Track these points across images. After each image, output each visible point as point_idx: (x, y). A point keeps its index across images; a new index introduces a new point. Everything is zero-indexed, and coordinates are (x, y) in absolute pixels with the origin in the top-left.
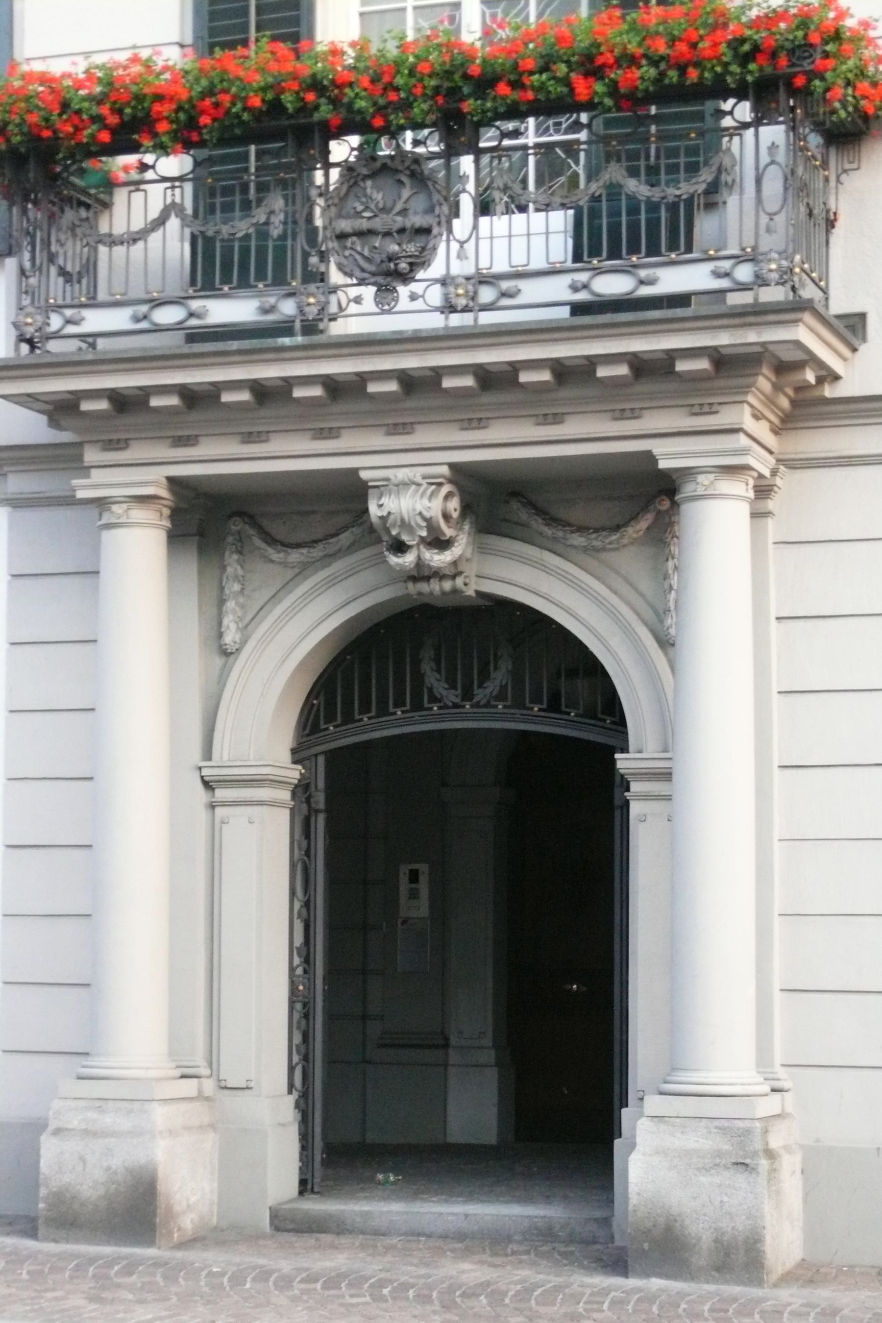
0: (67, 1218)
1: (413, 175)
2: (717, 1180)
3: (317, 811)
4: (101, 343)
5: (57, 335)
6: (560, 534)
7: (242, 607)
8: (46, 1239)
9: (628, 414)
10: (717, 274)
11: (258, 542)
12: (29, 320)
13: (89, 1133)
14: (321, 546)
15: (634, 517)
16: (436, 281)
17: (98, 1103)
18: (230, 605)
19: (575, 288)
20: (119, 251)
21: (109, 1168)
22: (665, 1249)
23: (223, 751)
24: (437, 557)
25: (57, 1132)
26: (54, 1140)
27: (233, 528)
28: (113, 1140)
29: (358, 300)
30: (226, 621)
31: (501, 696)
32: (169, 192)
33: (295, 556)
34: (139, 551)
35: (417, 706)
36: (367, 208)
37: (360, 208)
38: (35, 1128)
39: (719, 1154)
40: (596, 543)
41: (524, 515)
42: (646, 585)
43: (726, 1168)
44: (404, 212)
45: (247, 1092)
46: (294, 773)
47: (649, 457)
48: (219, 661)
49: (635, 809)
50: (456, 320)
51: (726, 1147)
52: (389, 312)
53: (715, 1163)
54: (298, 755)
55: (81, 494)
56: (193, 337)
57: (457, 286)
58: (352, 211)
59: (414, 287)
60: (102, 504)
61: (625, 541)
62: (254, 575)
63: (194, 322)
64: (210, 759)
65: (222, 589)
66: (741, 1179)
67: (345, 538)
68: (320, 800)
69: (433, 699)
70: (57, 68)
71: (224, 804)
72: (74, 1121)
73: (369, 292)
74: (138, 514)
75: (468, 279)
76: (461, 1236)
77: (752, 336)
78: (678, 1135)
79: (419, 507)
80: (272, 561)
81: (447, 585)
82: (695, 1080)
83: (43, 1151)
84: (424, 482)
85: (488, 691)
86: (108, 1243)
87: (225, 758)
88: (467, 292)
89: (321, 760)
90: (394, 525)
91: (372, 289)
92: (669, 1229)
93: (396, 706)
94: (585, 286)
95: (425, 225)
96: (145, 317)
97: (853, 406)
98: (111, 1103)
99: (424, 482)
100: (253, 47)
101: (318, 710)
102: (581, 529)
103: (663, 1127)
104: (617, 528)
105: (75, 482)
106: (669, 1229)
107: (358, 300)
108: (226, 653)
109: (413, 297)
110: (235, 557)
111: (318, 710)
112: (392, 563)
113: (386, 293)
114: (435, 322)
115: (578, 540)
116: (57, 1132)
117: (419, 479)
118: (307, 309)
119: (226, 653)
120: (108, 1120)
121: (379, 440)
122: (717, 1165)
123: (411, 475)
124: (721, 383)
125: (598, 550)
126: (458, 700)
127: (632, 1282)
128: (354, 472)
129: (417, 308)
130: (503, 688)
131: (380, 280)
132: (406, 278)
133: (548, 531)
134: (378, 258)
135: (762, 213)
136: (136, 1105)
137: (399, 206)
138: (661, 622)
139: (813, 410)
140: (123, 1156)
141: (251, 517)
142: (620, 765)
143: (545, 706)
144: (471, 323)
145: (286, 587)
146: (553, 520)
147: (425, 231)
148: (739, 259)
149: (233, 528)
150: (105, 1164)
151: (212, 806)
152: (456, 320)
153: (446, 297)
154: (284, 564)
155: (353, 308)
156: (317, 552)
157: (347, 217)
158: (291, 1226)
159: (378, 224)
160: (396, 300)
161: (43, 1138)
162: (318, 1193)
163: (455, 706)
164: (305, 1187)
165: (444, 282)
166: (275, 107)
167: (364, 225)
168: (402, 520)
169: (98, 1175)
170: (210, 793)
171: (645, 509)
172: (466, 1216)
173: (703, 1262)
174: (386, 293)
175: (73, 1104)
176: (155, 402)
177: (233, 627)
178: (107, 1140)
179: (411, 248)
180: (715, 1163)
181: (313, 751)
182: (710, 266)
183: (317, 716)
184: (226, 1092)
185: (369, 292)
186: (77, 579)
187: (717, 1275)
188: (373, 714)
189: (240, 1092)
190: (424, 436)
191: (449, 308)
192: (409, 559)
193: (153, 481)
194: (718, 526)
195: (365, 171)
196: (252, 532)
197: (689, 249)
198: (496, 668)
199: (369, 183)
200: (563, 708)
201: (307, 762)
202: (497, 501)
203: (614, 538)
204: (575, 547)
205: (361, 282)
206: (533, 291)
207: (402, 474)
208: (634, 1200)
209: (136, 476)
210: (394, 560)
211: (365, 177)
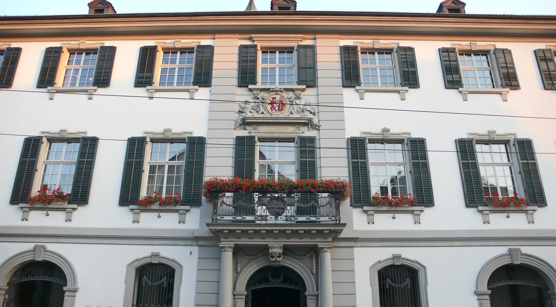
5: (219, 220)
15: (307, 254)
20: (322, 208)
23: (237, 289)
31: (282, 281)
33: (250, 257)
34: (228, 256)
35: (267, 283)
46: (246, 293)
50: (288, 222)
54: (247, 289)
60: (223, 247)
67: (259, 255)
68: (250, 298)
70: (224, 178)
73: (273, 217)
74: (230, 249)
100: (256, 43)
108: (237, 273)
113: (276, 218)
114: (285, 222)
115: (299, 257)
119: (237, 273)
121: (272, 240)
129: (281, 220)
132: (280, 215)
146: (294, 254)
151: (234, 299)
152: (288, 222)
156: (254, 257)
159: (275, 207)
165: (286, 216)
166: (262, 188)
174: (276, 218)
185: (273, 217)
191: (287, 220)
193: (232, 244)
194: (327, 256)
207: (275, 245)
209: (228, 244)
210: (271, 259)
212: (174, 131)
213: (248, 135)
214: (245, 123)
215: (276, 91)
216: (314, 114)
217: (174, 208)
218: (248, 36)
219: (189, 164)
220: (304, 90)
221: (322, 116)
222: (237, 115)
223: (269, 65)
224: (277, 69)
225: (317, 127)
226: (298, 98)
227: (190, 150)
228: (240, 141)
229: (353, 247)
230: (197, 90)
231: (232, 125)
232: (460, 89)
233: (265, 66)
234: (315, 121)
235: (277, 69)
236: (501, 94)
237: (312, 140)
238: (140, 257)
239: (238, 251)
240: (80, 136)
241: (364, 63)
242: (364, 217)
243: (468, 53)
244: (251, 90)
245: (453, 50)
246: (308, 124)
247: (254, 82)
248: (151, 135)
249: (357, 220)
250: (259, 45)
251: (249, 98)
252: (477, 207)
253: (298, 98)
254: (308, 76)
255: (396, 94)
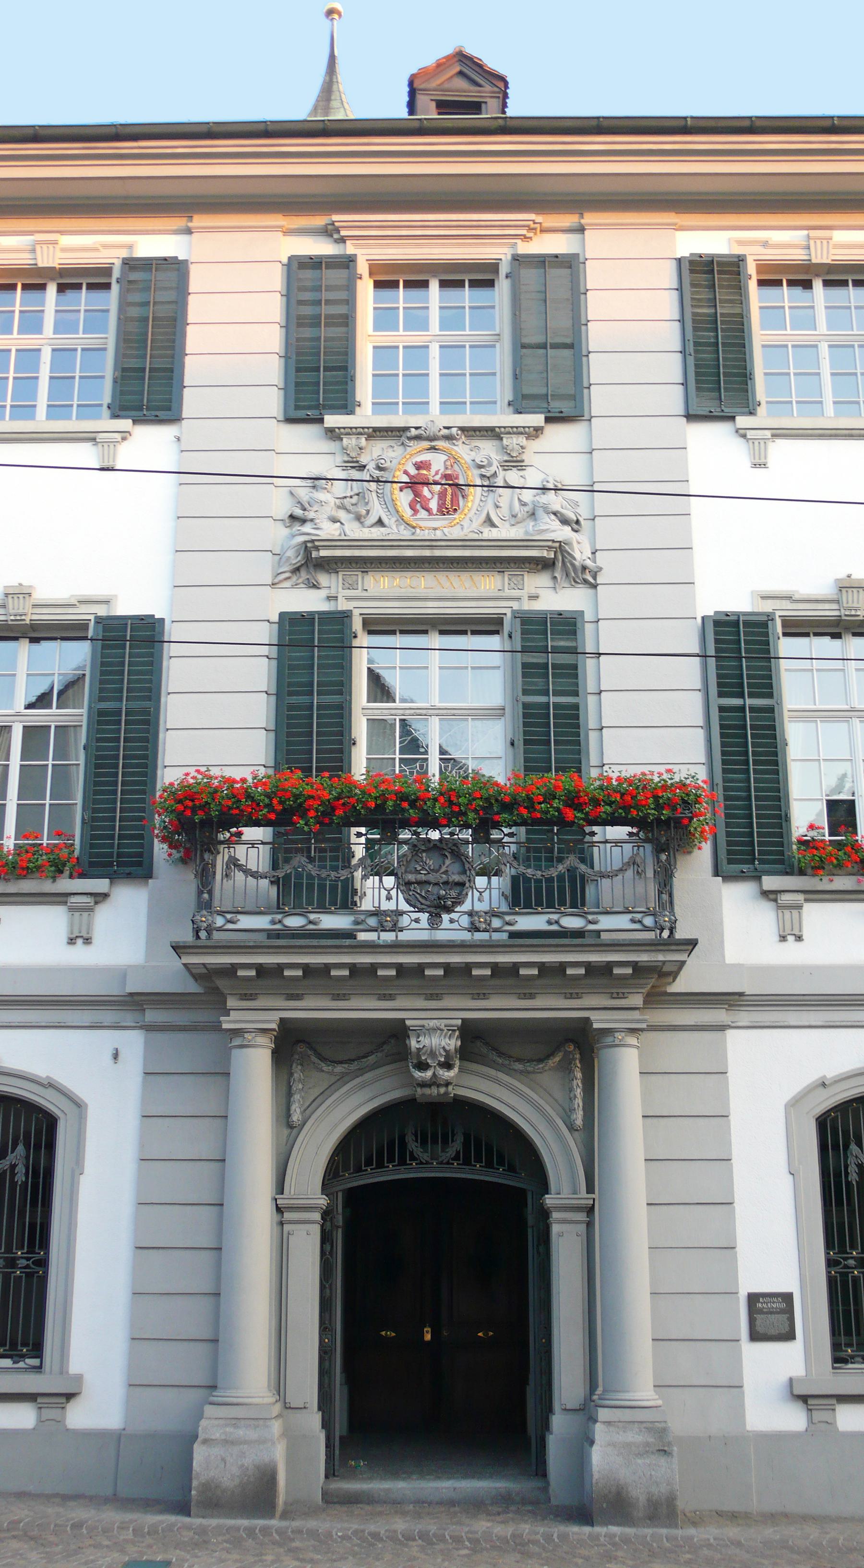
0: (215, 1502)
1: (452, 852)
2: (648, 1461)
3: (338, 1227)
4: (604, 936)
6: (507, 1062)
7: (303, 1098)
8: (198, 1516)
9: (481, 996)
10: (633, 921)
11: (314, 1059)
12: (204, 919)
13: (227, 1442)
14: (356, 1063)
16: (465, 913)
17: (234, 1422)
18: (297, 1097)
19: (549, 922)
20: (605, 883)
21: (243, 1466)
22: (616, 1506)
24: (446, 1074)
25: (205, 1441)
26: (204, 1448)
27: (299, 1049)
28: (246, 1446)
29: (417, 921)
30: (293, 1107)
31: (456, 1158)
32: (226, 850)
33: (339, 1069)
34: (256, 1064)
35: (402, 1162)
36: (423, 869)
37: (419, 868)
38: (188, 1440)
39: (647, 1444)
40: (529, 1069)
41: (484, 1050)
42: (558, 1095)
43: (652, 1453)
44: (446, 872)
45: (304, 1410)
47: (587, 1020)
48: (286, 1131)
49: (555, 1229)
50: (479, 936)
51: (651, 1440)
52: (437, 929)
53: (645, 1451)
55: (225, 1026)
56: (513, 935)
57: (479, 917)
58: (413, 870)
59: (454, 916)
60: (237, 1032)
61: (547, 1068)
62: (308, 1081)
63: (311, 927)
64: (282, 1193)
65: (290, 1087)
66: (663, 1461)
67: (372, 1059)
68: (340, 1220)
69: (413, 1158)
70: (237, 774)
71: (291, 1222)
72: (217, 1435)
75: (486, 913)
76: (452, 1503)
77: (661, 957)
78: (621, 1433)
79: (443, 1044)
80: (323, 1071)
81: (442, 1090)
82: (627, 1398)
83: (195, 1455)
84: (445, 1029)
85: (448, 1155)
86: (242, 1517)
87: (292, 1193)
88: (486, 920)
89: (340, 1195)
90: (424, 1054)
91: (427, 915)
92: (619, 1494)
93: (389, 1161)
94: (557, 922)
95: (461, 881)
96: (280, 922)
97: (678, 998)
98: (243, 1422)
99: (445, 1029)
100: (350, 248)
101: (338, 1163)
102: (519, 1060)
103: (611, 1429)
104: (540, 1061)
105: (222, 1018)
106: (619, 1494)
107: (417, 921)
108: (290, 1126)
109: (452, 921)
110: (299, 1067)
111: (338, 1163)
112: (416, 1076)
114: (466, 936)
115: (518, 1066)
116: (205, 1441)
117: (442, 1027)
118: (386, 924)
119: (290, 1126)
120: (241, 1433)
121: (421, 1003)
122: (647, 1452)
123: (438, 1024)
124: (636, 981)
125: (529, 1072)
126: (428, 1159)
127: (598, 1529)
128: (403, 1021)
130: (458, 1153)
131: (432, 909)
132: (449, 910)
133: (500, 1061)
134: (432, 897)
135: (382, 890)
136: (261, 1422)
137: (444, 869)
138: (569, 1117)
139: (658, 998)
140: (252, 1457)
141: (309, 1043)
142: (548, 1201)
143: (461, 1162)
144: (488, 938)
145: (331, 1089)
146: (501, 1054)
147: (462, 884)
148: (646, 913)
149: (299, 1049)
150: (240, 1463)
151: (281, 1224)
152: (479, 936)
153: (472, 923)
154: (330, 1073)
155: (414, 925)
156: (354, 1066)
157: (411, 872)
158: (335, 1500)
159: (431, 878)
160: (441, 922)
161: (195, 1446)
162: (338, 1476)
163: (427, 1163)
164: (330, 1473)
165: (471, 914)
167: (424, 878)
168: (432, 1051)
169: (235, 1470)
170: (280, 1215)
171: (557, 1049)
172: (455, 1489)
173: (641, 1514)
175: (216, 1422)
176: (241, 973)
177: (298, 1110)
178: (241, 1446)
179: (453, 893)
180: (645, 1451)
181: (335, 1189)
182: (630, 916)
183: (337, 1168)
184: (290, 1411)
186: (192, 1077)
187: (649, 1522)
188: (374, 1166)
189: (299, 1411)
190: (448, 1002)
192: (429, 1074)
193: (272, 1020)
195: (423, 848)
196: (310, 1052)
197: (583, 904)
198: (453, 1141)
199: (424, 854)
200: (495, 1166)
201: (331, 1196)
202: (479, 1042)
203: (541, 1066)
204: (515, 1070)
205: (420, 911)
206: (246, 922)
207: (432, 1023)
208: (596, 1476)
210: (418, 1074)
211: (424, 851)
212: (42, 594)
213: (325, 607)
214: (313, 563)
215: (429, 439)
216: (576, 525)
217: (48, 886)
218: (319, 221)
219: (102, 719)
220: (538, 430)
221: (608, 533)
222: (282, 532)
223: (401, 337)
224: (435, 351)
225: (586, 577)
226: (515, 463)
227: (107, 670)
228: (295, 631)
229: (722, 1028)
230: (125, 435)
231: (263, 569)
232: (742, 421)
233: (386, 338)
234: (581, 553)
235: (435, 351)
236: (94, 439)
237: (568, 625)
238: (831, 1072)
239: (293, 1046)
240: (87, 613)
241: (772, 323)
242: (765, 917)
243: (800, 277)
244: (333, 434)
245: (732, 267)
246: (552, 562)
247: (346, 403)
248: (786, 605)
249: (737, 928)
250: (365, 255)
251: (325, 461)
252: (758, 878)
253: (515, 463)
254: (551, 378)
255: (88, 445)
